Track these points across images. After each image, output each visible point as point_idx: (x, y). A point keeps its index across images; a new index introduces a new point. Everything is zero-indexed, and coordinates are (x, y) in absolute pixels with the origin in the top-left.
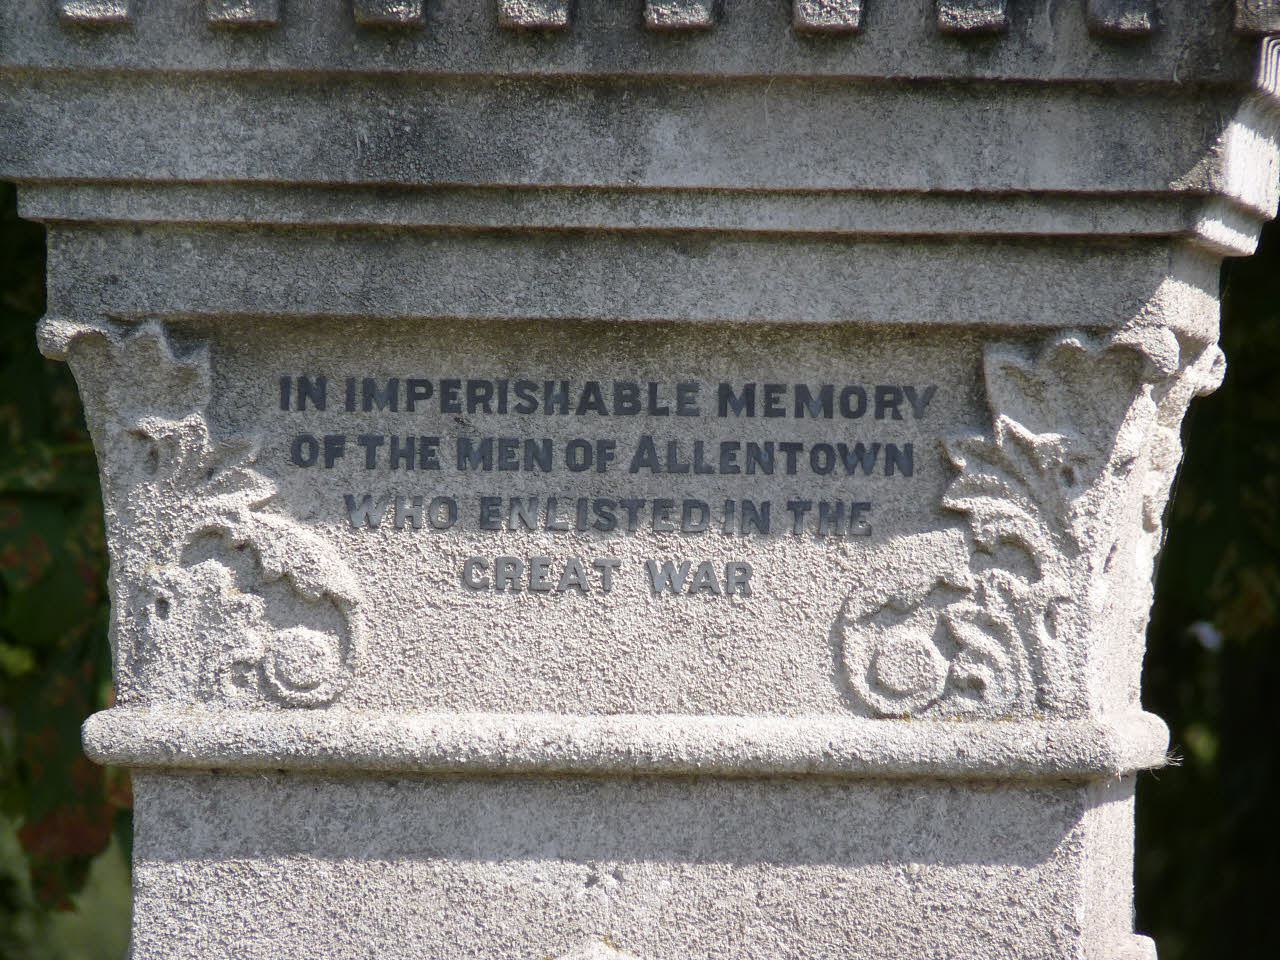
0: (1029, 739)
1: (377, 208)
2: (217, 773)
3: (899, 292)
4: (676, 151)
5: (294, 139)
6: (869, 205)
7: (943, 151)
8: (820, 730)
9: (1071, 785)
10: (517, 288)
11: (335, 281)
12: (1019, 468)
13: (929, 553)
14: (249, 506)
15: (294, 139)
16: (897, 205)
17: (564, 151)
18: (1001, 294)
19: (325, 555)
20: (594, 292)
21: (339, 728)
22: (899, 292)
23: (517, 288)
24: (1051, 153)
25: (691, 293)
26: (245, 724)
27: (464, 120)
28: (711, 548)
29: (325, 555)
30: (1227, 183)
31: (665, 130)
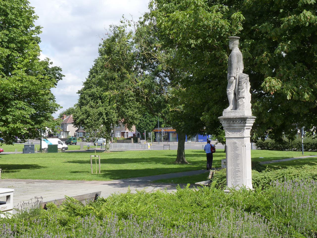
0: (243, 136)
1: (230, 126)
2: (227, 137)
3: (240, 127)
4: (235, 125)
5: (228, 125)
6: (74, 174)
7: (240, 125)
8: (239, 136)
9: (244, 120)
10: (232, 128)
11: (229, 128)
12: (242, 131)
13: (241, 133)
14: (228, 132)
15: (228, 125)
16: (84, 173)
17: (233, 125)
18: (242, 127)
19: (229, 133)
20: (234, 128)
21: (229, 137)
22: (240, 127)
23: (232, 128)
24: (242, 125)
25: (235, 128)
26: (228, 137)
27: (231, 124)
28: (237, 133)
29: (229, 133)
30: (52, 95)
31: (235, 124)
